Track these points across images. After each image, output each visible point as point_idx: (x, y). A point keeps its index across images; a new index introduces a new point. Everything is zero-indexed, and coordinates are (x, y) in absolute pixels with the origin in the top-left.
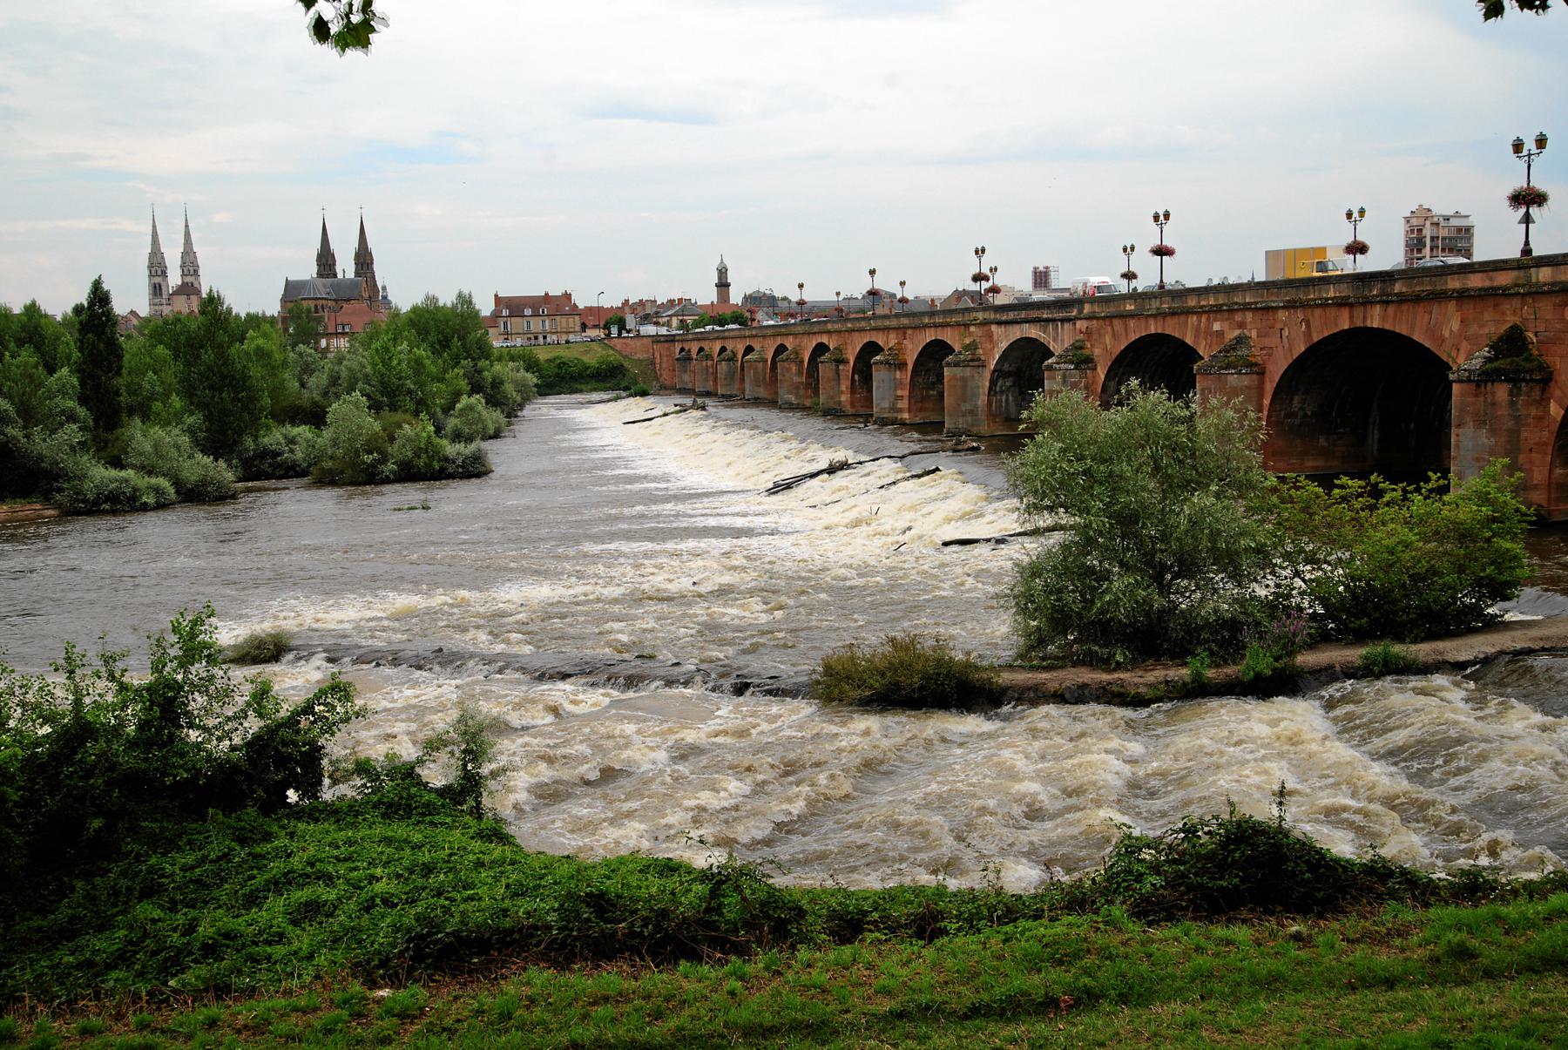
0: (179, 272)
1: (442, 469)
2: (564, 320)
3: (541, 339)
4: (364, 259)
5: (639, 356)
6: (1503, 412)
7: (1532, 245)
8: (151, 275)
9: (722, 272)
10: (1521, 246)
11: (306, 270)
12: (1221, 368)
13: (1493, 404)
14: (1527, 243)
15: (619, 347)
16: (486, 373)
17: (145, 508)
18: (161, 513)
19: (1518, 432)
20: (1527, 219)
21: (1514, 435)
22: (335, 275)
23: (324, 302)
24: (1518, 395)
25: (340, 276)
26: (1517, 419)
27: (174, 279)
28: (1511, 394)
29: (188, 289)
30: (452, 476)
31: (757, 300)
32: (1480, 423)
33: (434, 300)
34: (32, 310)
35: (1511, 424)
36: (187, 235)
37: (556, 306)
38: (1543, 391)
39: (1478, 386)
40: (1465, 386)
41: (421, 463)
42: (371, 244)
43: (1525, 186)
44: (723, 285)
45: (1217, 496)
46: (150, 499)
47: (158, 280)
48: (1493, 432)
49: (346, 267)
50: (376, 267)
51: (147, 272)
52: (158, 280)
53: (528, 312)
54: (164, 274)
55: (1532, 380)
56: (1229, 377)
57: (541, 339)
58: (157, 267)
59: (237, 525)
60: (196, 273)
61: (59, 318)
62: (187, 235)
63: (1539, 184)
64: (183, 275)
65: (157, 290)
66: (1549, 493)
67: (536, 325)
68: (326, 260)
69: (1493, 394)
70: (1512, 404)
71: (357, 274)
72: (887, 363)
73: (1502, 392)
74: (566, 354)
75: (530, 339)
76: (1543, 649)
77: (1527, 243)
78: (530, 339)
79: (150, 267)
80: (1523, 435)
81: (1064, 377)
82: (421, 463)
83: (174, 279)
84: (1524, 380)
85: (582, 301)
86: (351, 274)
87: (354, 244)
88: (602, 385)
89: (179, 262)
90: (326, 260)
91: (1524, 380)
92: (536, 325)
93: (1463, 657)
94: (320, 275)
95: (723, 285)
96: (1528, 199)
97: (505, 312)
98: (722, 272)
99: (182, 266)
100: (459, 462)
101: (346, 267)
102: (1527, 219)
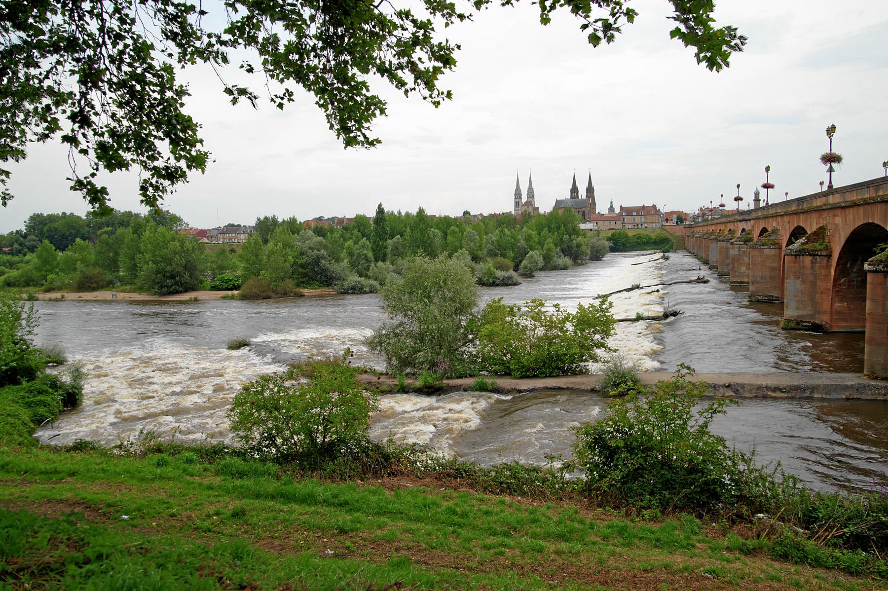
1: (494, 282)
2: (651, 217)
3: (640, 226)
4: (590, 190)
5: (678, 234)
6: (808, 272)
7: (833, 183)
10: (587, 184)
11: (566, 195)
12: (760, 245)
13: (803, 267)
14: (830, 182)
15: (669, 230)
16: (574, 241)
17: (365, 293)
18: (371, 295)
19: (815, 282)
20: (831, 170)
21: (814, 284)
22: (578, 197)
24: (816, 263)
26: (815, 276)
27: (524, 199)
28: (812, 262)
29: (529, 203)
30: (497, 285)
32: (797, 277)
34: (64, 213)
35: (812, 278)
36: (530, 181)
37: (651, 211)
38: (828, 261)
39: (796, 257)
40: (790, 257)
41: (485, 279)
43: (829, 152)
46: (367, 289)
47: (518, 200)
48: (803, 282)
49: (582, 194)
50: (595, 193)
52: (518, 200)
53: (634, 214)
54: (520, 198)
55: (822, 255)
56: (765, 250)
57: (640, 226)
58: (518, 194)
60: (533, 197)
62: (530, 181)
63: (836, 151)
66: (831, 316)
67: (638, 219)
68: (574, 190)
69: (803, 262)
70: (813, 268)
71: (587, 196)
72: (716, 239)
73: (808, 260)
74: (642, 232)
76: (568, 388)
77: (830, 182)
80: (818, 284)
81: (739, 248)
82: (485, 279)
83: (524, 199)
84: (817, 255)
85: (664, 210)
86: (584, 197)
88: (656, 247)
90: (574, 190)
91: (817, 255)
92: (638, 219)
93: (522, 388)
96: (831, 159)
97: (624, 214)
100: (501, 279)
101: (582, 194)
102: (831, 170)
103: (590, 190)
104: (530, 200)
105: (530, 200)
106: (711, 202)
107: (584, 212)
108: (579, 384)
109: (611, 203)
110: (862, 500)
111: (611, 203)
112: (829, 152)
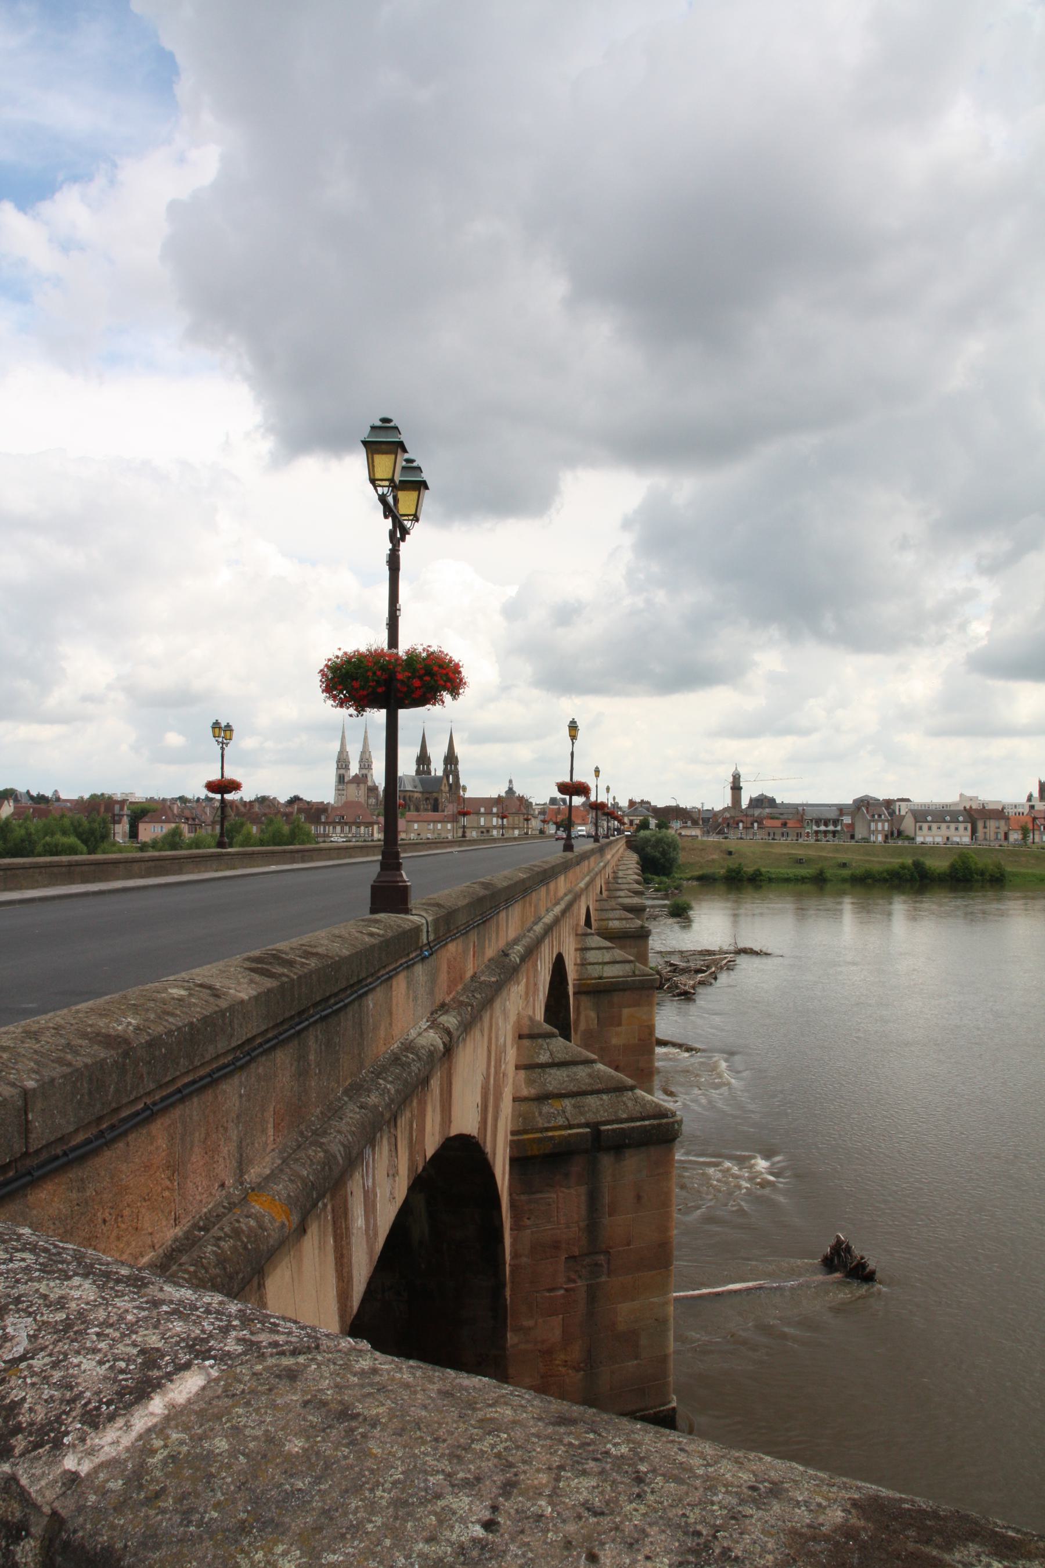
0: (358, 766)
4: (451, 759)
8: (338, 768)
9: (736, 779)
22: (429, 773)
23: (411, 794)
25: (433, 774)
27: (354, 769)
31: (761, 802)
33: (82, 798)
42: (458, 750)
44: (736, 788)
45: (179, 1453)
47: (342, 771)
49: (437, 768)
50: (460, 767)
51: (335, 766)
52: (342, 771)
58: (343, 762)
59: (840, 900)
60: (369, 767)
61: (517, 794)
64: (361, 768)
65: (341, 779)
71: (445, 770)
75: (482, 832)
78: (482, 832)
79: (339, 761)
86: (440, 773)
87: (445, 749)
89: (358, 759)
94: (418, 772)
95: (736, 788)
98: (736, 779)
99: (361, 761)
101: (437, 768)
103: (451, 759)
104: (364, 771)
105: (364, 771)
106: (597, 772)
107: (436, 800)
108: (544, 993)
109: (511, 782)
110: (374, 941)
111: (511, 782)
112: (375, 639)
